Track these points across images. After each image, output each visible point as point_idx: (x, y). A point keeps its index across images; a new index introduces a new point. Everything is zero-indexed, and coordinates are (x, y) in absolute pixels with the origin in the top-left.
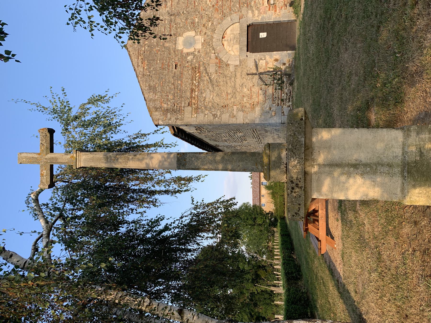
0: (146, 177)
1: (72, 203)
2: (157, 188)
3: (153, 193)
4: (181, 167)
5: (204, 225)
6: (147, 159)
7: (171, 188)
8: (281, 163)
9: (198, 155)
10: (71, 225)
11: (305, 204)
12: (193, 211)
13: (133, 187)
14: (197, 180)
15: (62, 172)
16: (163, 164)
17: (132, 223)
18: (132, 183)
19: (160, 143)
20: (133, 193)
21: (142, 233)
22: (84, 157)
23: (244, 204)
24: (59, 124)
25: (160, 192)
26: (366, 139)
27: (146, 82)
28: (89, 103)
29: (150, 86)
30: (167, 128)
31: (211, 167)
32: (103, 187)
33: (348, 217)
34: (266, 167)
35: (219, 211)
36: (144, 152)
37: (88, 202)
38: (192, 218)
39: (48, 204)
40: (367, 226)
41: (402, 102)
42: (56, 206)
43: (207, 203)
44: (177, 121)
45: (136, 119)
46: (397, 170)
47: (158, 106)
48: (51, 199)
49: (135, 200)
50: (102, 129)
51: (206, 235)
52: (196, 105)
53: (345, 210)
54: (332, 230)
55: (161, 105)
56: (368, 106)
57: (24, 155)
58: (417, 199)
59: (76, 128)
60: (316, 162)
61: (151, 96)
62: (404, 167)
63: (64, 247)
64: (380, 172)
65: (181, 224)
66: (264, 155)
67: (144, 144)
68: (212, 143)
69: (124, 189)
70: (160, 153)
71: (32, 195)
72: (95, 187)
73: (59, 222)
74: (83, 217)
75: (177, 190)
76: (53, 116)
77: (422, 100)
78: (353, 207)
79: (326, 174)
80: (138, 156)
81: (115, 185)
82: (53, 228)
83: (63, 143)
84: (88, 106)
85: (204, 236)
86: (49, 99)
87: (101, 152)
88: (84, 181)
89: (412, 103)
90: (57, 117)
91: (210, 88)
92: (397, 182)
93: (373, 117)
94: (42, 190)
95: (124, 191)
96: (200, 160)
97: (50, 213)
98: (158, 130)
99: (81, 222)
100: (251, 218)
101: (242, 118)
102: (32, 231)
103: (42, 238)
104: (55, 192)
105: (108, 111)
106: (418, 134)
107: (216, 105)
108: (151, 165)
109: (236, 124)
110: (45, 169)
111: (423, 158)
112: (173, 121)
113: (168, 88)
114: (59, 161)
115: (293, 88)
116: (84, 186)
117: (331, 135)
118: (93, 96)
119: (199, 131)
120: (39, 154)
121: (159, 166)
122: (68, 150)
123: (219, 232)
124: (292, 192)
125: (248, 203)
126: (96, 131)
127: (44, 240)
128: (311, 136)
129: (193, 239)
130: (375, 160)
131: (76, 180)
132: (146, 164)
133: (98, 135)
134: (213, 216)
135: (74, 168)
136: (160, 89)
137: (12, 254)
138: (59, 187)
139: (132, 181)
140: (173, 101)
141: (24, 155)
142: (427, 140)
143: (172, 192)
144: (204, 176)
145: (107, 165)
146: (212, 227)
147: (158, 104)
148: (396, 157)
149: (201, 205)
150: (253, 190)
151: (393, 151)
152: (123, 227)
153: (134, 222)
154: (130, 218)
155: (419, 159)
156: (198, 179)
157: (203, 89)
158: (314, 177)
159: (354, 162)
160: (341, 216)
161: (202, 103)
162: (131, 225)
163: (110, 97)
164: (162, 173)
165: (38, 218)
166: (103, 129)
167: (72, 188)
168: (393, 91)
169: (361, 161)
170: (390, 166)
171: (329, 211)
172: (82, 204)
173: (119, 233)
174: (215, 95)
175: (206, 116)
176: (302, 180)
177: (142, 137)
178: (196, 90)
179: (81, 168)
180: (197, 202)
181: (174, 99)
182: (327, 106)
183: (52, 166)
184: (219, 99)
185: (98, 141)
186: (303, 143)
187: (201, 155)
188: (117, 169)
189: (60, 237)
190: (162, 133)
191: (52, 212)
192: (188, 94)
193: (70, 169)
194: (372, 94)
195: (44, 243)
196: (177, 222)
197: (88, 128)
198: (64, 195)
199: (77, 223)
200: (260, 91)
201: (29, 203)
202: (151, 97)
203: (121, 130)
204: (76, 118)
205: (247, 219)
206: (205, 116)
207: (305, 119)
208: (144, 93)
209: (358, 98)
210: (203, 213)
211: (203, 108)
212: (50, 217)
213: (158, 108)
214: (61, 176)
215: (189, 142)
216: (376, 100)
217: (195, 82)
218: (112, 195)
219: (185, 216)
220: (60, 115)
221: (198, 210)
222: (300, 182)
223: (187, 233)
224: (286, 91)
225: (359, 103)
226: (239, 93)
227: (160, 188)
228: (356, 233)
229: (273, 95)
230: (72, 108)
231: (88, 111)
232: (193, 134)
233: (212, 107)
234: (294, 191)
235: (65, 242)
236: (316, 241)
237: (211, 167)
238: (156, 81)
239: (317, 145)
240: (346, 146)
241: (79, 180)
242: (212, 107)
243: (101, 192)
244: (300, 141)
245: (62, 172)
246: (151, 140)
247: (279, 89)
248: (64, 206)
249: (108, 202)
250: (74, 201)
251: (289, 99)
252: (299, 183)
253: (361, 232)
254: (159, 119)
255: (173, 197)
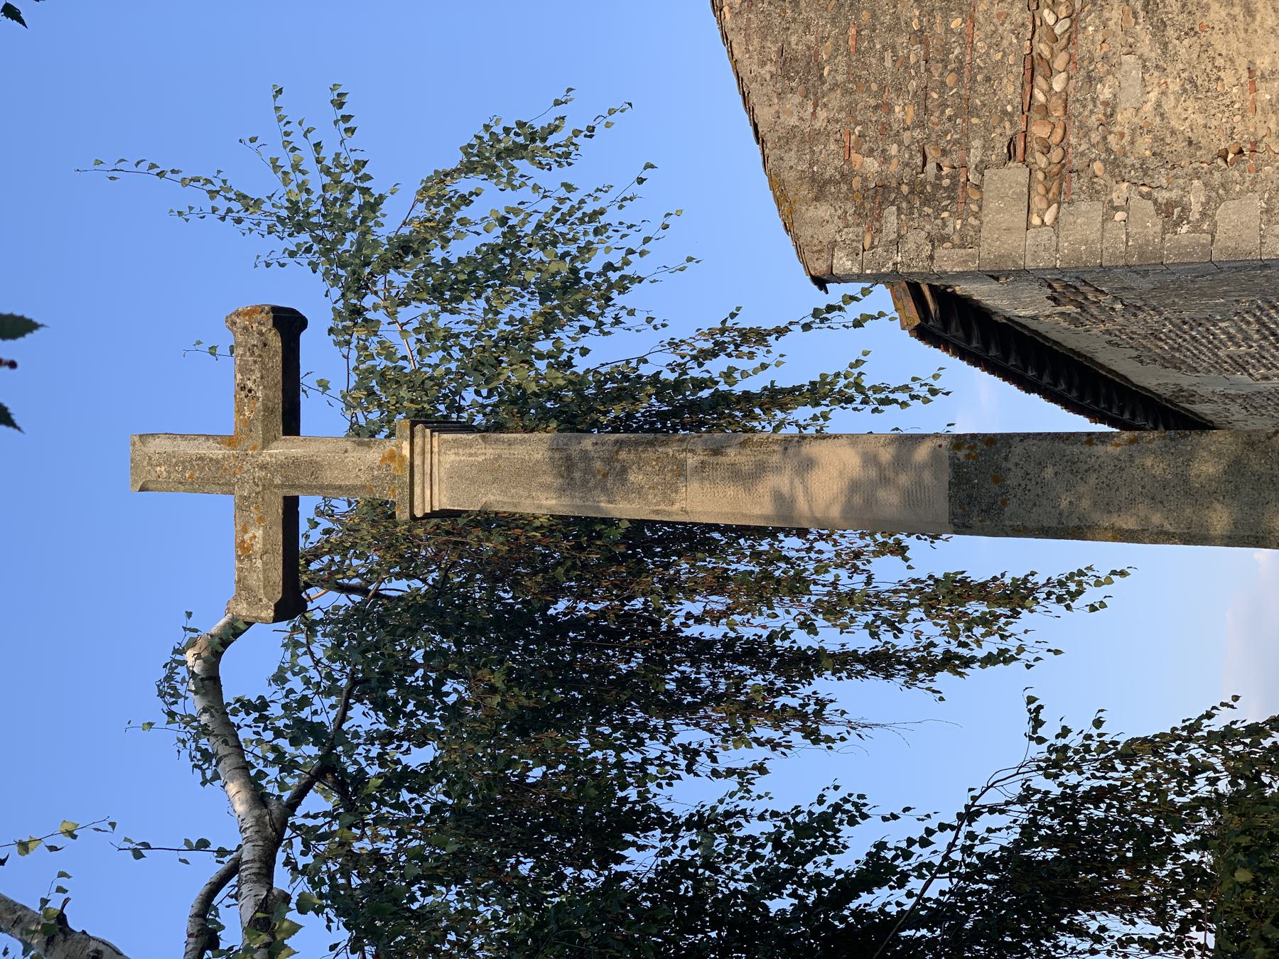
0: (767, 576)
1: (380, 705)
2: (830, 638)
3: (805, 664)
4: (975, 520)
5: (1106, 868)
6: (778, 469)
7: (905, 642)
9: (1076, 449)
10: (379, 820)
12: (1040, 783)
13: (693, 630)
14: (1060, 599)
15: (334, 538)
16: (870, 501)
17: (689, 824)
18: (688, 606)
19: (842, 382)
20: (695, 663)
21: (743, 886)
22: (451, 457)
24: (317, 284)
25: (844, 663)
27: (764, 38)
28: (468, 169)
29: (786, 61)
30: (881, 298)
31: (1156, 519)
32: (535, 626)
35: (1201, 787)
36: (753, 430)
37: (461, 701)
38: (1033, 821)
39: (263, 705)
42: (305, 713)
43: (1122, 740)
44: (940, 252)
45: (711, 250)
47: (830, 171)
48: (279, 678)
49: (705, 702)
50: (531, 308)
51: (1115, 925)
52: (1056, 155)
55: (848, 161)
57: (158, 446)
59: (404, 302)
61: (793, 112)
63: (343, 936)
65: (967, 850)
67: (754, 385)
68: (1151, 378)
69: (644, 635)
70: (853, 439)
71: (189, 656)
72: (498, 623)
73: (317, 802)
74: (438, 780)
75: (938, 652)
76: (291, 244)
80: (732, 455)
81: (602, 614)
82: (288, 833)
83: (339, 384)
84: (464, 185)
85: (1103, 929)
86: (268, 154)
87: (526, 430)
88: (440, 589)
90: (308, 250)
91: (1146, 45)
94: (237, 633)
95: (644, 652)
96: (1092, 479)
97: (275, 749)
98: (830, 308)
99: (427, 808)
102: (187, 842)
103: (234, 881)
104: (297, 644)
105: (565, 208)
107: (1181, 146)
108: (802, 505)
110: (261, 519)
112: (913, 254)
113: (888, 63)
114: (329, 477)
116: (442, 613)
118: (487, 127)
119: (1071, 309)
120: (230, 441)
121: (848, 509)
122: (362, 421)
123: (1197, 914)
126: (504, 317)
127: (245, 889)
129: (1037, 943)
131: (402, 584)
132: (778, 497)
133: (516, 341)
134: (1158, 815)
135: (402, 515)
136: (843, 68)
137: (98, 952)
138: (318, 615)
139: (690, 594)
140: (917, 134)
141: (158, 446)
143: (910, 664)
144: (1103, 574)
145: (565, 501)
146: (1157, 880)
147: (829, 158)
149: (1087, 749)
152: (641, 848)
153: (699, 822)
154: (685, 796)
156: (1067, 590)
157: (1098, 54)
161: (1095, 137)
162: (686, 838)
163: (576, 133)
164: (857, 555)
165: (216, 776)
166: (536, 304)
167: (383, 624)
172: (429, 709)
173: (623, 876)
174: (1175, 86)
175: (1120, 216)
177: (745, 349)
178: (1060, 62)
179: (433, 514)
180: (1065, 732)
181: (921, 125)
183: (291, 505)
184: (1203, 111)
185: (512, 374)
187: (1100, 449)
188: (609, 522)
189: (322, 882)
190: (858, 324)
191: (284, 743)
192: (1009, 90)
193: (374, 524)
195: (247, 908)
196: (941, 841)
197: (464, 305)
198: (342, 658)
199: (407, 810)
201: (176, 695)
202: (793, 121)
203: (631, 313)
204: (404, 248)
206: (1107, 218)
208: (753, 99)
210: (1096, 796)
211: (1097, 167)
212: (273, 772)
213: (830, 181)
214: (326, 559)
215: (1007, 375)
217: (1049, 18)
218: (586, 667)
219: (992, 810)
220: (320, 240)
221: (1072, 778)
223: (1003, 906)
227: (845, 638)
230: (381, 198)
231: (464, 212)
232: (1033, 325)
233: (1153, 163)
235: (347, 908)
237: (1156, 519)
238: (822, 24)
241: (416, 583)
242: (1153, 163)
243: (525, 648)
245: (334, 538)
246: (796, 362)
248: (343, 718)
249: (559, 706)
250: (391, 692)
254: (833, 245)
255: (917, 694)
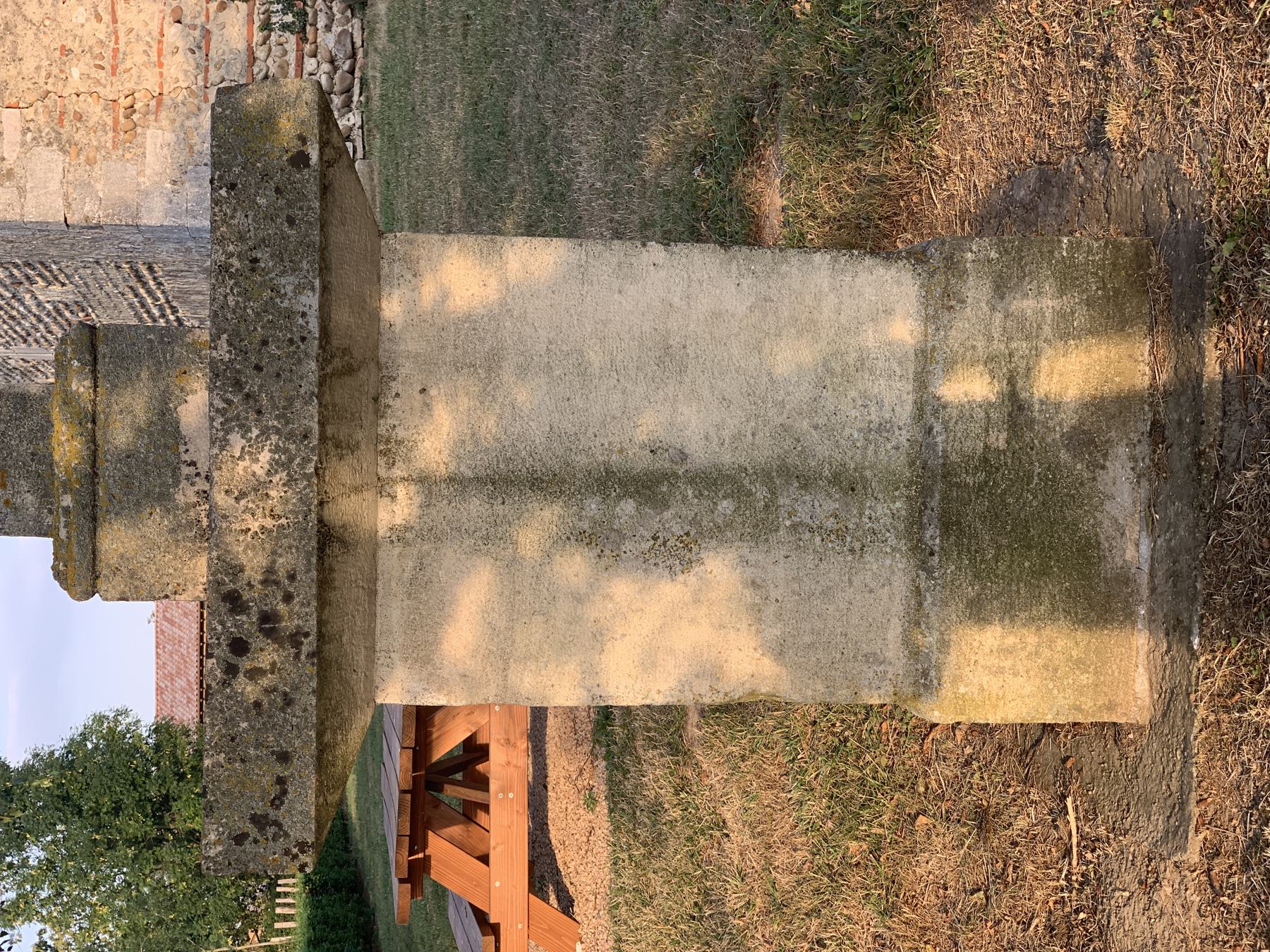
8: (175, 471)
11: (323, 748)
23: (100, 719)
26: (717, 315)
33: (643, 786)
34: (67, 501)
40: (740, 837)
41: (922, 106)
46: (887, 510)
53: (628, 748)
54: (567, 859)
56: (743, 139)
58: (993, 684)
60: (407, 460)
62: (925, 492)
64: (794, 527)
66: (56, 414)
77: (1024, 97)
78: (670, 723)
79: (469, 542)
89: (975, 113)
92: (879, 586)
93: (773, 200)
100: (140, 803)
101: (54, 186)
106: (1001, 289)
109: (21, 226)
111: (1028, 436)
115: (368, 29)
117: (504, 280)
124: (231, 670)
125: (126, 713)
128: (376, 279)
130: (765, 451)
142: (1047, 331)
148: (881, 428)
150: (160, 632)
151: (864, 395)
155: (1002, 444)
158: (391, 562)
159: (642, 462)
160: (610, 781)
168: (876, 42)
169: (683, 456)
170: (848, 484)
171: (551, 748)
176: (306, 588)
182: (543, 136)
186: (314, 325)
194: (768, 59)
200: (173, 31)
205: (117, 810)
207: (326, 163)
209: (699, 88)
216: (790, 97)
222: (288, 598)
224: (328, 41)
225: (699, 119)
226: (39, 28)
228: (685, 877)
229: (253, 59)
234: (245, 664)
236: (475, 930)
239: (411, 344)
240: (595, 358)
244: (289, 314)
247: (285, 27)
251: (348, 91)
252: (282, 607)
253: (705, 875)
